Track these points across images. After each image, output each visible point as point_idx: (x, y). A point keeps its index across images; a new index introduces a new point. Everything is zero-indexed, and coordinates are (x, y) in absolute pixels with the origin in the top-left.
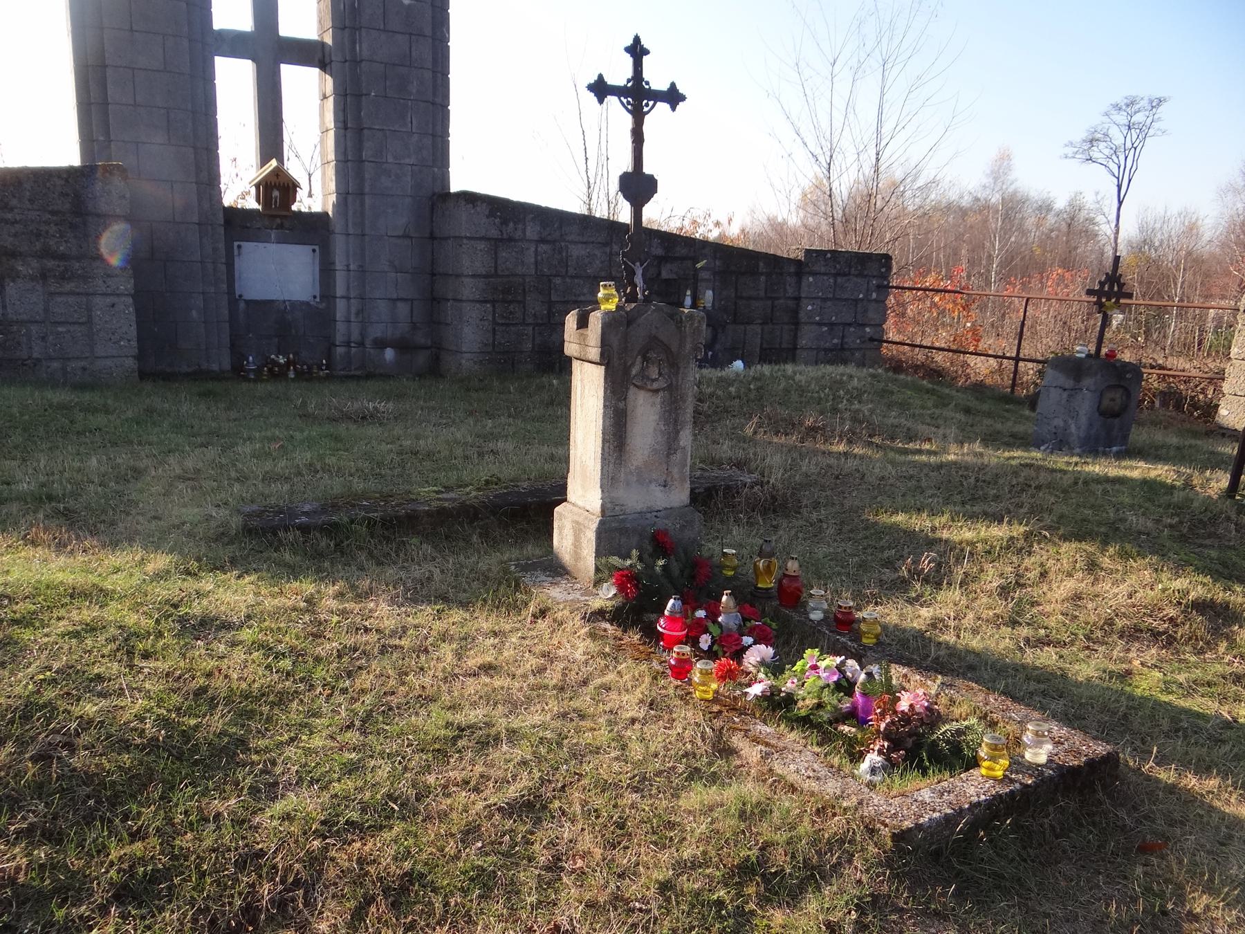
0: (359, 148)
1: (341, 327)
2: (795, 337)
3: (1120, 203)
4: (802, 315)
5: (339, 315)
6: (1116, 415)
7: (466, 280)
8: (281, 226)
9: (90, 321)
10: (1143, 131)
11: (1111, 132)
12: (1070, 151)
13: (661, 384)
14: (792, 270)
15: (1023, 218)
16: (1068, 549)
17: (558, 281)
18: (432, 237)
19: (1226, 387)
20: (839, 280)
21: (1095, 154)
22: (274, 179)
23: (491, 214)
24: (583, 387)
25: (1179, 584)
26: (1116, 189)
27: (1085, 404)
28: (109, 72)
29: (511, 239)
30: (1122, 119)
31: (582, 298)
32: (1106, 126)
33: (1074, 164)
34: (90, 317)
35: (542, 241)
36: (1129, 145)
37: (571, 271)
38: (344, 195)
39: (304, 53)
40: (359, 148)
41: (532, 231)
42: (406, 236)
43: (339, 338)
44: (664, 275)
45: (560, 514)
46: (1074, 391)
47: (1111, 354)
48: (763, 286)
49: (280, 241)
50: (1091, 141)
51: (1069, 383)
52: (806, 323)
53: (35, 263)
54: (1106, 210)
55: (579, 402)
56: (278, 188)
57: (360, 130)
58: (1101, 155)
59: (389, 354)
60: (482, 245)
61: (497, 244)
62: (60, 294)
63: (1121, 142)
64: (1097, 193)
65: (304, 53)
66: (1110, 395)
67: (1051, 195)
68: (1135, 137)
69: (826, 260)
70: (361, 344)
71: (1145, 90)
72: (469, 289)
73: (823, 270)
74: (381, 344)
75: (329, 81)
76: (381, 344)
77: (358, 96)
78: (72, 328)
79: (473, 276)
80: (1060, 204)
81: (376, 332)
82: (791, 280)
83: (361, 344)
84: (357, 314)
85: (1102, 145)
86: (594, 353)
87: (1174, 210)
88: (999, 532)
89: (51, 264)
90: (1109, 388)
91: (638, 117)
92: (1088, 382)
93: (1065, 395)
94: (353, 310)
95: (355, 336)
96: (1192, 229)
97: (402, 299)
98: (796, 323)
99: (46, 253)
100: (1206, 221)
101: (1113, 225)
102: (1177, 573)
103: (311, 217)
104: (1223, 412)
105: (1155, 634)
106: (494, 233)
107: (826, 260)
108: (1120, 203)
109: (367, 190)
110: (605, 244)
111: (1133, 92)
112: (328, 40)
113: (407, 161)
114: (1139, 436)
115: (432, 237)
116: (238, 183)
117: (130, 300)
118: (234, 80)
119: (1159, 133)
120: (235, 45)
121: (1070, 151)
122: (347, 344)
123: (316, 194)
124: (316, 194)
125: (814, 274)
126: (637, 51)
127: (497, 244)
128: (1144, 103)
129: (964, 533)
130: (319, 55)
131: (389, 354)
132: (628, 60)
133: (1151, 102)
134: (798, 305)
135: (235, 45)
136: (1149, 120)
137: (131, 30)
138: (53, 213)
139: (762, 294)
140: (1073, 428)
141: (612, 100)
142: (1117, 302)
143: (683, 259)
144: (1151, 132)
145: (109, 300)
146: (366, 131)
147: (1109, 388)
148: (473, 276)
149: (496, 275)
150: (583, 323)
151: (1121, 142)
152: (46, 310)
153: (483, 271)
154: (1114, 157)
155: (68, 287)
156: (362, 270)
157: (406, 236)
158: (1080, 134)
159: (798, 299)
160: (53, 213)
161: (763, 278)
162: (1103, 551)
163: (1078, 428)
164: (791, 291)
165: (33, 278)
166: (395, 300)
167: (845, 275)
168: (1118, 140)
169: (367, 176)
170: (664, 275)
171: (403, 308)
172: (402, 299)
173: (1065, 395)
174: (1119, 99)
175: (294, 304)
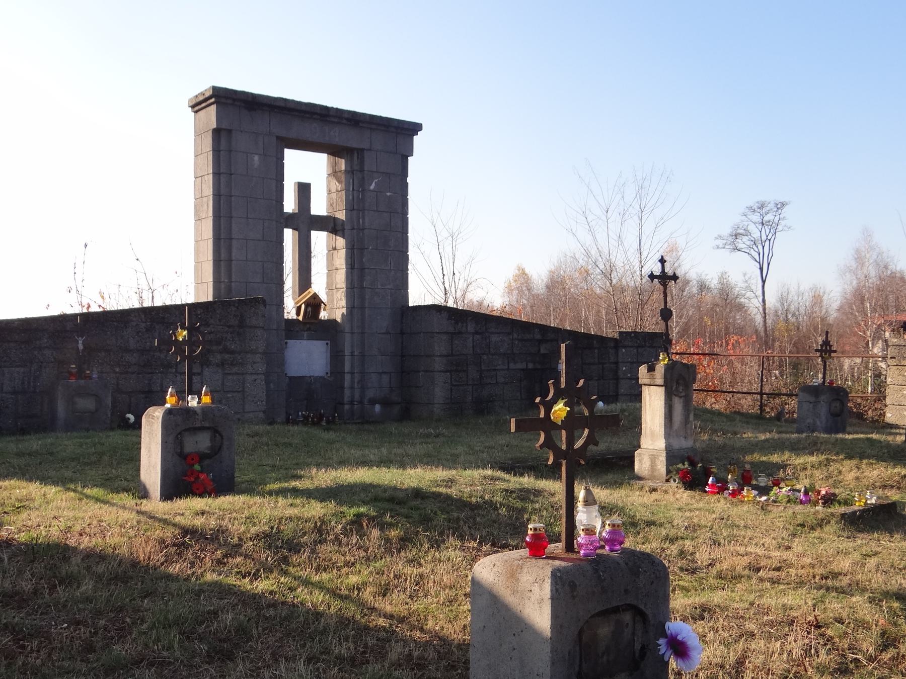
0: (361, 278)
1: (347, 392)
2: (617, 388)
3: (764, 282)
4: (620, 373)
5: (347, 384)
6: (838, 415)
7: (437, 359)
8: (309, 329)
9: (243, 391)
10: (773, 227)
11: (749, 228)
12: (720, 243)
13: (683, 394)
14: (612, 345)
15: (823, 319)
16: (847, 463)
17: (485, 357)
18: (402, 333)
19: (888, 401)
20: (640, 350)
21: (740, 246)
22: (312, 300)
23: (449, 318)
24: (650, 397)
25: (896, 470)
26: (759, 271)
27: (823, 410)
28: (234, 242)
29: (460, 333)
30: (756, 218)
31: (498, 367)
32: (746, 223)
33: (725, 253)
34: (244, 388)
35: (477, 333)
36: (764, 238)
37: (492, 351)
38: (351, 308)
39: (328, 224)
40: (361, 278)
41: (471, 327)
42: (387, 333)
43: (346, 399)
44: (542, 351)
45: (640, 454)
46: (816, 403)
47: (831, 383)
48: (596, 355)
49: (310, 338)
50: (736, 235)
51: (812, 399)
52: (623, 379)
53: (219, 356)
54: (753, 287)
55: (647, 403)
56: (314, 304)
57: (362, 269)
58: (744, 246)
59: (378, 408)
60: (444, 337)
61: (453, 335)
62: (230, 374)
63: (759, 233)
64: (745, 275)
65: (328, 224)
66: (834, 405)
67: (703, 277)
68: (768, 231)
69: (631, 338)
70: (361, 402)
71: (771, 197)
72: (438, 364)
73: (630, 344)
74: (373, 402)
75: (341, 242)
76: (373, 402)
77: (362, 249)
78: (235, 394)
79: (440, 356)
80: (713, 282)
81: (370, 393)
82: (612, 351)
83: (361, 402)
84: (358, 383)
85: (745, 239)
86: (660, 381)
87: (806, 286)
88: (813, 459)
89: (227, 356)
90: (833, 400)
91: (665, 286)
92: (823, 398)
93: (811, 406)
94: (356, 380)
95: (357, 397)
96: (817, 300)
97: (385, 373)
98: (617, 379)
99: (226, 350)
100: (832, 295)
101: (761, 299)
102: (895, 466)
103: (332, 323)
104: (888, 415)
105: (892, 487)
106: (451, 329)
107: (631, 338)
108: (764, 282)
109: (367, 305)
110: (509, 334)
111: (762, 198)
112: (341, 215)
113: (389, 287)
114: (849, 429)
115: (402, 333)
116: (290, 307)
117: (263, 377)
118: (289, 235)
119: (786, 229)
120: (290, 221)
121: (720, 243)
122: (352, 403)
123: (335, 309)
124: (335, 309)
125: (625, 347)
126: (662, 261)
127: (453, 335)
128: (772, 206)
129: (799, 461)
130: (332, 225)
131: (378, 408)
132: (659, 264)
133: (777, 205)
134: (617, 367)
135: (290, 221)
136: (777, 218)
137: (247, 218)
138: (229, 327)
139: (596, 361)
140: (818, 423)
141: (656, 280)
142: (830, 355)
143: (552, 341)
144: (780, 228)
145: (254, 377)
146: (367, 270)
147: (833, 400)
148: (440, 356)
149: (452, 355)
150: (651, 369)
151: (759, 233)
152: (223, 384)
153: (445, 353)
154: (754, 247)
155: (235, 369)
156: (363, 355)
157: (387, 333)
158: (727, 231)
159: (617, 363)
160: (229, 327)
161: (596, 351)
162: (861, 463)
163: (821, 422)
164: (612, 359)
165: (218, 365)
166: (380, 374)
167: (642, 347)
168: (756, 235)
169: (367, 297)
170: (542, 351)
171: (385, 378)
172: (385, 373)
173: (811, 406)
174: (752, 201)
175: (317, 378)
